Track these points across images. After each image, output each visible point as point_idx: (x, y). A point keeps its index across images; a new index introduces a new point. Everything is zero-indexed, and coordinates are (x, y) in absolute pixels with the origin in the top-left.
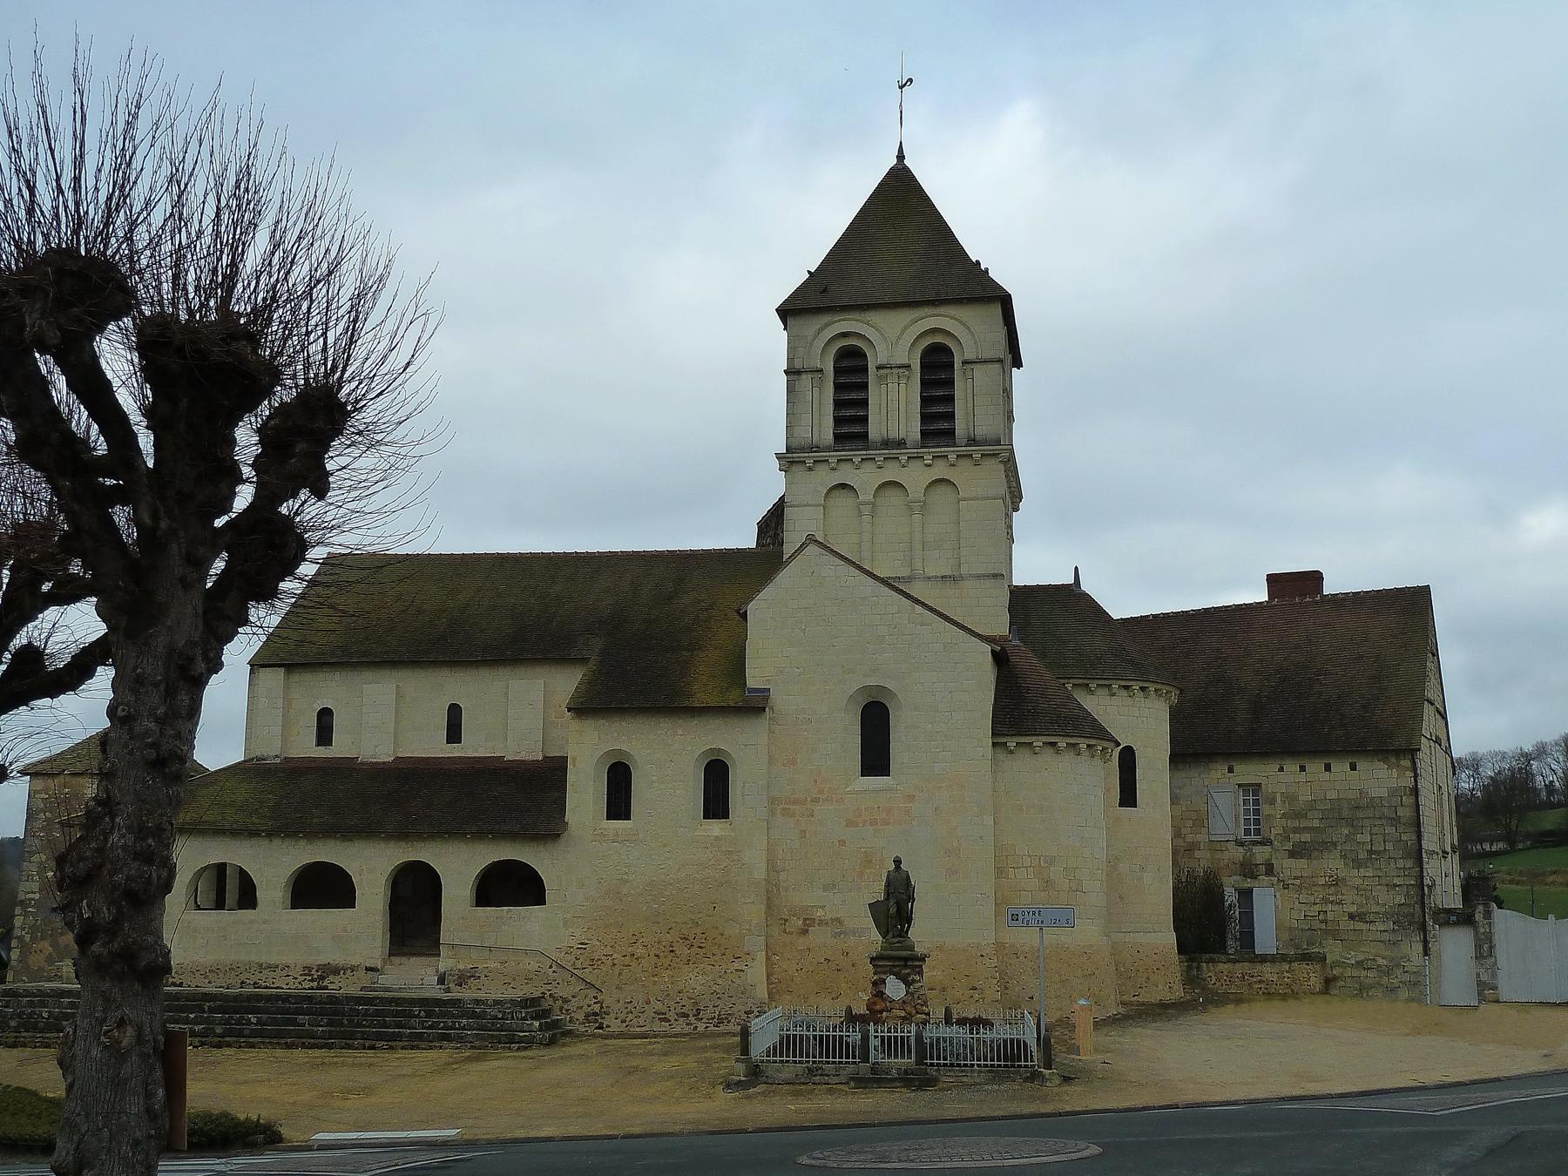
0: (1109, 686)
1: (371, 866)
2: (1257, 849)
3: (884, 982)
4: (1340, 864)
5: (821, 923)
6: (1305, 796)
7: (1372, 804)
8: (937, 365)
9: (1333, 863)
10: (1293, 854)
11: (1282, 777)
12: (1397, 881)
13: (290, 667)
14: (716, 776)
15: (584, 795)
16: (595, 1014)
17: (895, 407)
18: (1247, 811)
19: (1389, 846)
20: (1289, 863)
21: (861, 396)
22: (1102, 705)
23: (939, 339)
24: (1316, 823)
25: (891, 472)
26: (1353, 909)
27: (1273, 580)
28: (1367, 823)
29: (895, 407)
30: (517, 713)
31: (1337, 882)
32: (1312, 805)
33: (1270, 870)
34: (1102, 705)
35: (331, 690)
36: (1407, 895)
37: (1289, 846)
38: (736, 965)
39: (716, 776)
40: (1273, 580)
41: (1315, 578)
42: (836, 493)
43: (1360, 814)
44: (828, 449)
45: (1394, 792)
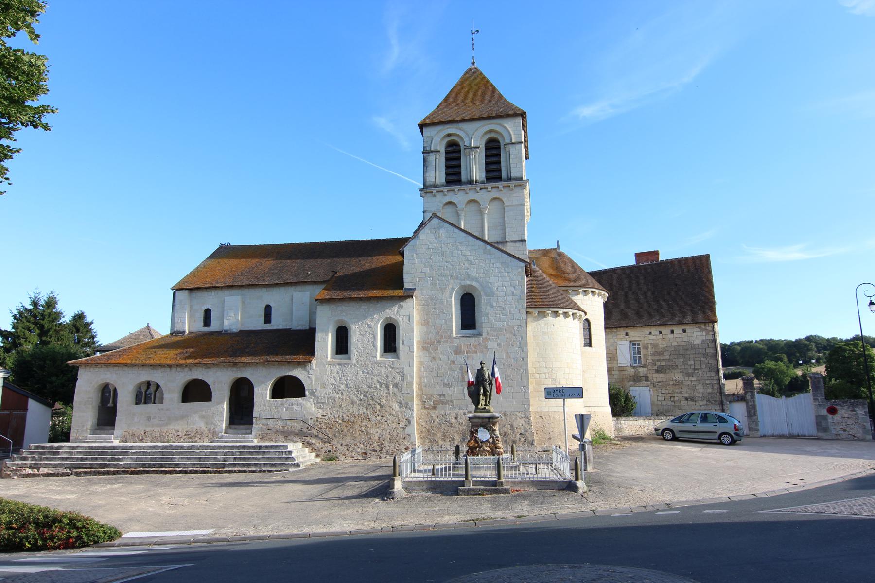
0: (577, 291)
1: (220, 381)
2: (641, 370)
3: (477, 431)
4: (680, 375)
6: (662, 345)
7: (694, 347)
8: (494, 150)
9: (677, 375)
10: (657, 371)
11: (651, 337)
12: (708, 382)
13: (191, 290)
14: (390, 334)
15: (326, 341)
17: (475, 167)
18: (634, 353)
19: (703, 366)
20: (656, 375)
21: (457, 170)
22: (579, 299)
23: (493, 135)
24: (668, 357)
25: (472, 195)
26: (687, 395)
27: (637, 255)
29: (475, 167)
30: (290, 306)
31: (679, 384)
32: (666, 349)
33: (647, 378)
34: (579, 299)
35: (210, 300)
36: (712, 388)
37: (655, 368)
39: (390, 334)
40: (637, 255)
41: (656, 253)
42: (447, 206)
43: (688, 352)
44: (443, 186)
45: (703, 342)
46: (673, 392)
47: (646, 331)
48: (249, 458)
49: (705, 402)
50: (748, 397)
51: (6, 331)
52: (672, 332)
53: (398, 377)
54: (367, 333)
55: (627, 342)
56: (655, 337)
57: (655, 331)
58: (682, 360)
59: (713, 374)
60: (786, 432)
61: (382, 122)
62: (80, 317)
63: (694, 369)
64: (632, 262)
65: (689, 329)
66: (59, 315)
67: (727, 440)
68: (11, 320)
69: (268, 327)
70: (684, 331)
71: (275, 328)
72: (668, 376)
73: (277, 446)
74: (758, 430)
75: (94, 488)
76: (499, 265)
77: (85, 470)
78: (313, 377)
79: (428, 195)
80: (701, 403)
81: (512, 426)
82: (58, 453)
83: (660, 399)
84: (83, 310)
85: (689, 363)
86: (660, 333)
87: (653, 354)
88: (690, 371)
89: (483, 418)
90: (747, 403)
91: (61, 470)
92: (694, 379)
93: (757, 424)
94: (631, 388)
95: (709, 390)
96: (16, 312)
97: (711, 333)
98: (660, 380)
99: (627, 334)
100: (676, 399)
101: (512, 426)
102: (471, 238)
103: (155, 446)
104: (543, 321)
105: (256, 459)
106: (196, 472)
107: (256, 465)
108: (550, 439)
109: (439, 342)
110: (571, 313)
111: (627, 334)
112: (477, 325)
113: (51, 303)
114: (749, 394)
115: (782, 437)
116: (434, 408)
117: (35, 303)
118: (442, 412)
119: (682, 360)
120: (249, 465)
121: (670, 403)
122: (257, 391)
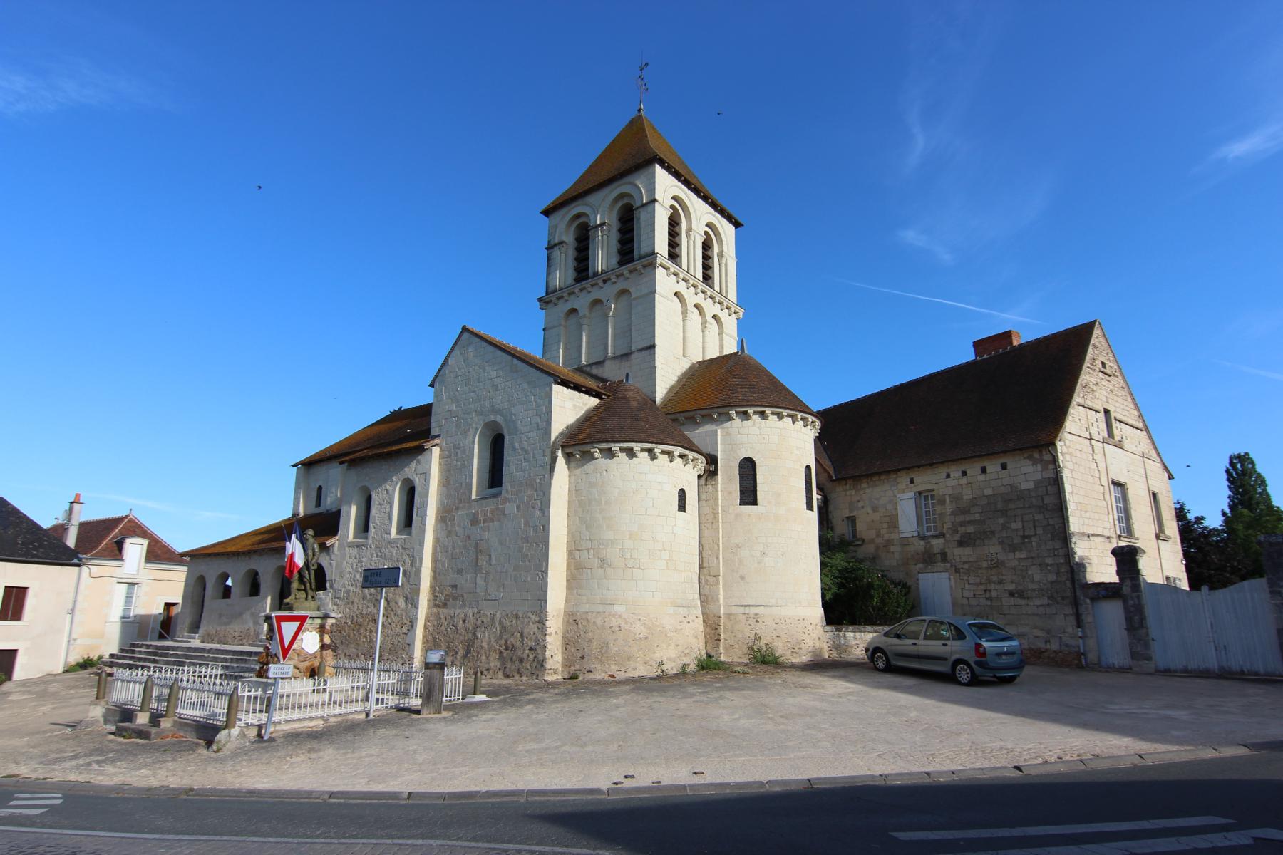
0: (710, 416)
2: (934, 542)
6: (967, 495)
9: (993, 549)
10: (961, 544)
11: (950, 482)
12: (1049, 561)
19: (1040, 531)
23: (626, 201)
24: (977, 517)
26: (1012, 587)
27: (977, 344)
31: (997, 565)
37: (957, 537)
40: (977, 344)
41: (1007, 335)
43: (1012, 506)
45: (1038, 484)
46: (989, 581)
47: (940, 473)
49: (1045, 601)
50: (1126, 589)
52: (984, 470)
53: (408, 561)
54: (390, 500)
55: (911, 495)
56: (954, 483)
57: (955, 471)
58: (1001, 521)
59: (1058, 544)
60: (1213, 663)
61: (910, 236)
63: (1024, 537)
64: (968, 355)
65: (1012, 462)
67: (964, 676)
70: (1004, 467)
74: (1149, 659)
76: (525, 386)
78: (334, 563)
79: (550, 305)
80: (1038, 602)
81: (522, 635)
83: (966, 594)
85: (1014, 526)
86: (964, 473)
87: (953, 513)
88: (1017, 540)
90: (1125, 602)
92: (1024, 555)
93: (1147, 646)
94: (921, 576)
95: (1052, 577)
97: (1051, 466)
98: (964, 559)
99: (912, 481)
100: (994, 594)
101: (522, 635)
102: (499, 353)
104: (590, 466)
108: (583, 657)
109: (457, 509)
110: (676, 453)
111: (912, 481)
114: (1128, 582)
115: (1204, 674)
116: (445, 606)
118: (451, 612)
119: (1001, 521)
121: (983, 602)
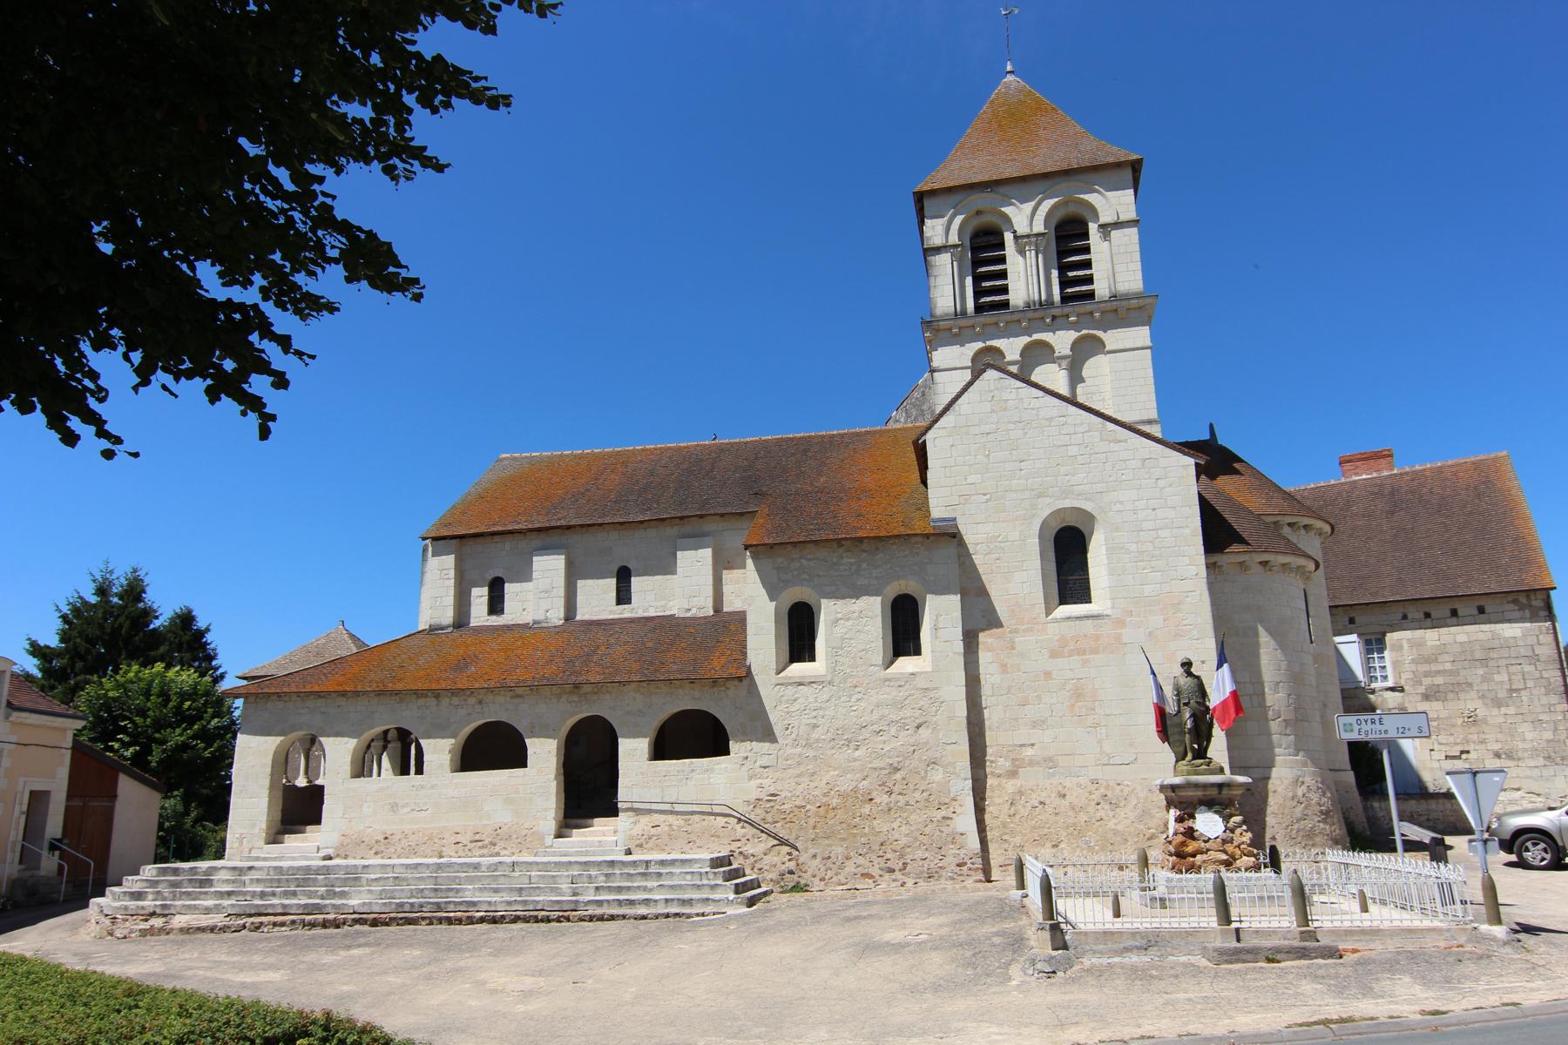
4: (1478, 704)
5: (1032, 763)
9: (1470, 702)
16: (791, 872)
17: (1025, 277)
24: (1448, 666)
26: (1496, 747)
28: (1503, 662)
37: (1422, 689)
38: (943, 813)
43: (1494, 655)
48: (629, 888)
49: (1541, 761)
51: (47, 647)
58: (1480, 672)
62: (185, 620)
63: (1511, 690)
66: (149, 614)
68: (58, 624)
69: (625, 612)
71: (640, 614)
72: (1451, 705)
73: (684, 862)
75: (311, 957)
77: (272, 918)
80: (1532, 763)
82: (209, 882)
84: (192, 606)
88: (1502, 694)
89: (1205, 786)
91: (217, 919)
95: (1549, 735)
96: (66, 609)
103: (418, 865)
105: (645, 889)
106: (516, 919)
107: (647, 902)
111: (1352, 621)
112: (280, 794)
113: (135, 590)
117: (102, 591)
120: (631, 903)
122: (625, 745)
